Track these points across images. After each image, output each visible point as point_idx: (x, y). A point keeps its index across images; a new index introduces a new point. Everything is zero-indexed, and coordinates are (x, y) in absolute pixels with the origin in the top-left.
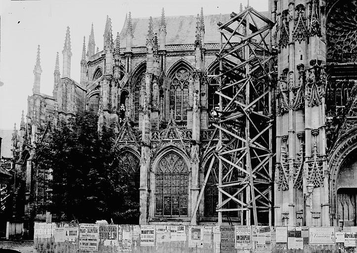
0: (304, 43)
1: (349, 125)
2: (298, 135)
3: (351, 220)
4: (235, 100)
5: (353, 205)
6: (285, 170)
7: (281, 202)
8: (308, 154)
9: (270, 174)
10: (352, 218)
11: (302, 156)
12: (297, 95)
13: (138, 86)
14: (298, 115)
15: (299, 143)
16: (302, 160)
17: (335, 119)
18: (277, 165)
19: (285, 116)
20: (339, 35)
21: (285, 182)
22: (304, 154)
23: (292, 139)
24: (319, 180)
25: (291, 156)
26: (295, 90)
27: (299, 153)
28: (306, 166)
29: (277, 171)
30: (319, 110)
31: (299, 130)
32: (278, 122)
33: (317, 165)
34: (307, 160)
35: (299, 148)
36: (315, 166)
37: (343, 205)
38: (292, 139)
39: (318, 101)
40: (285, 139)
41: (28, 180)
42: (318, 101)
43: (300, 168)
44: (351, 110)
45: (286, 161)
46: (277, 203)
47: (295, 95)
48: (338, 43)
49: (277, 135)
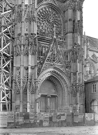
0: (28, 23)
1: (46, 66)
2: (25, 67)
3: (44, 109)
4: (8, 29)
5: (45, 102)
6: (18, 84)
7: (15, 100)
8: (29, 78)
9: (10, 85)
10: (44, 109)
11: (26, 78)
12: (25, 48)
13: (58, 29)
14: (25, 58)
15: (25, 71)
16: (26, 80)
17: (40, 62)
18: (14, 81)
19: (19, 57)
20: (42, 17)
21: (18, 90)
22: (28, 77)
23: (22, 69)
24: (34, 90)
25: (22, 77)
26: (24, 46)
27: (25, 76)
28: (29, 83)
29: (14, 84)
30: (35, 57)
31: (25, 65)
32: (14, 60)
33: (34, 84)
34: (29, 80)
35: (25, 74)
36: (33, 84)
37: (41, 102)
38: (22, 69)
39: (34, 53)
40: (18, 69)
41: (35, 23)
42: (34, 53)
43: (25, 84)
44: (46, 59)
45: (19, 79)
46: (13, 100)
47: (24, 47)
48: (42, 21)
49: (14, 65)
